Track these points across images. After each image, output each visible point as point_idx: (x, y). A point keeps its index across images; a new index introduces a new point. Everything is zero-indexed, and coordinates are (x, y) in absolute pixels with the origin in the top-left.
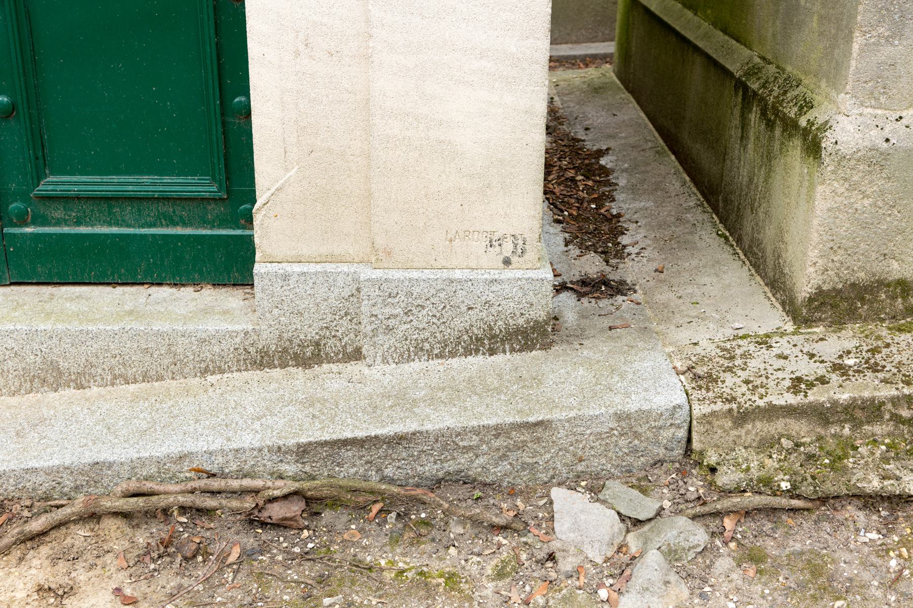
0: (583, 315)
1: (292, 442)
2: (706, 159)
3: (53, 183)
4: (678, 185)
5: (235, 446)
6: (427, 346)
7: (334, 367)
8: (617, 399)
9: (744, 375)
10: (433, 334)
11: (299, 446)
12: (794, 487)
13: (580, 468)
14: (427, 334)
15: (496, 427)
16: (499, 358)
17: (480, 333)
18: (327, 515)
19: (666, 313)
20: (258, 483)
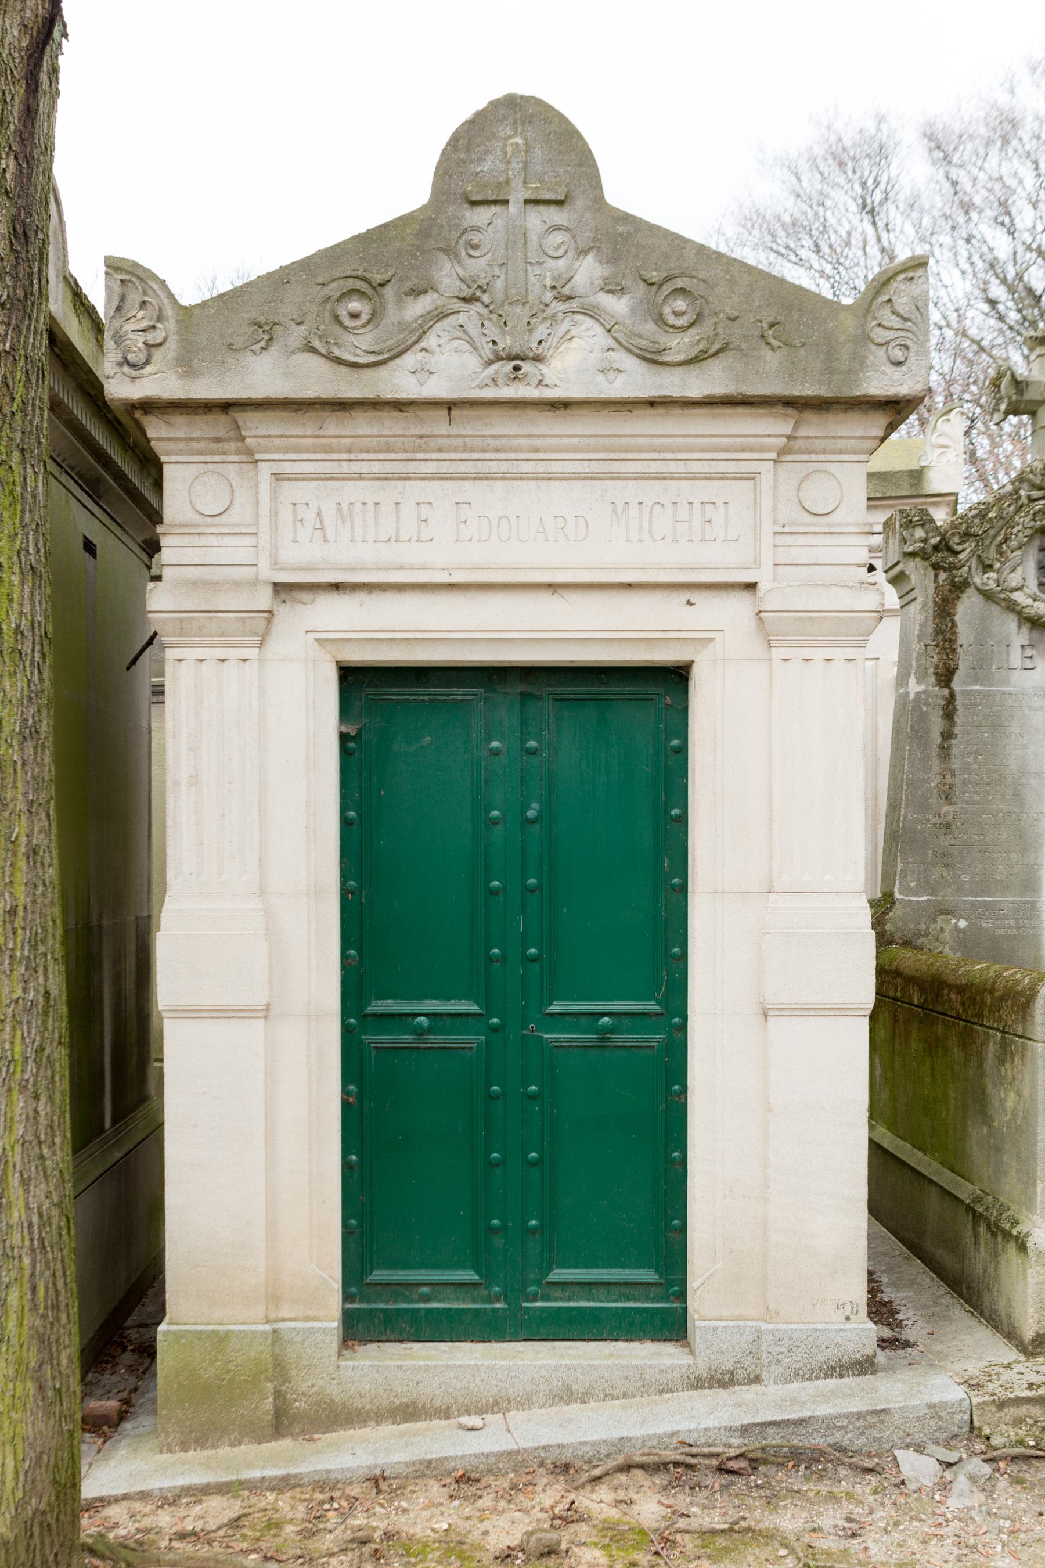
0: (889, 1358)
1: (738, 1424)
2: (948, 1260)
3: (559, 1274)
4: (928, 1280)
5: (704, 1426)
6: (801, 1373)
7: (743, 1387)
8: (926, 1397)
9: (999, 1383)
10: (805, 1365)
11: (742, 1426)
12: (1037, 1444)
13: (908, 1440)
14: (801, 1365)
15: (858, 1413)
16: (846, 1380)
17: (834, 1364)
18: (762, 1469)
19: (942, 1356)
20: (719, 1450)
